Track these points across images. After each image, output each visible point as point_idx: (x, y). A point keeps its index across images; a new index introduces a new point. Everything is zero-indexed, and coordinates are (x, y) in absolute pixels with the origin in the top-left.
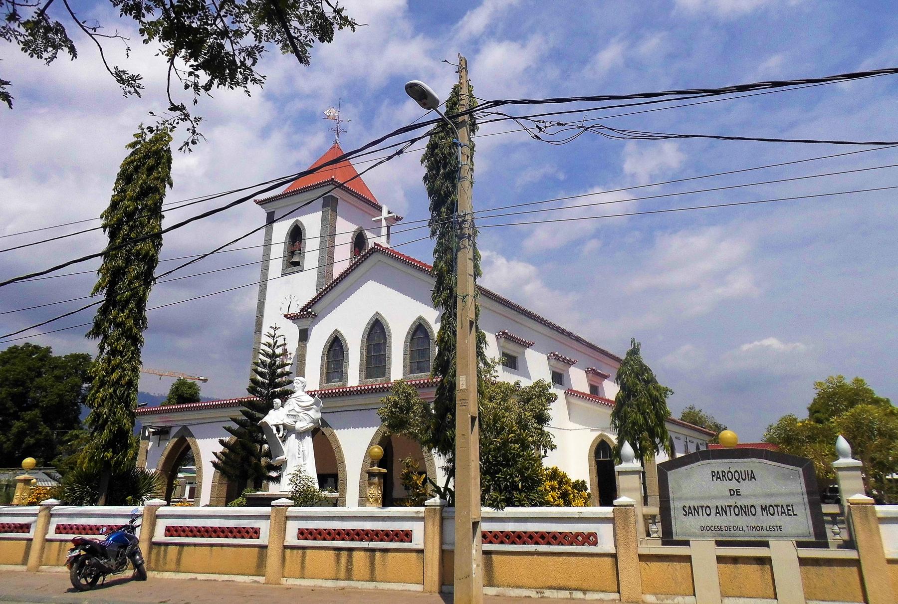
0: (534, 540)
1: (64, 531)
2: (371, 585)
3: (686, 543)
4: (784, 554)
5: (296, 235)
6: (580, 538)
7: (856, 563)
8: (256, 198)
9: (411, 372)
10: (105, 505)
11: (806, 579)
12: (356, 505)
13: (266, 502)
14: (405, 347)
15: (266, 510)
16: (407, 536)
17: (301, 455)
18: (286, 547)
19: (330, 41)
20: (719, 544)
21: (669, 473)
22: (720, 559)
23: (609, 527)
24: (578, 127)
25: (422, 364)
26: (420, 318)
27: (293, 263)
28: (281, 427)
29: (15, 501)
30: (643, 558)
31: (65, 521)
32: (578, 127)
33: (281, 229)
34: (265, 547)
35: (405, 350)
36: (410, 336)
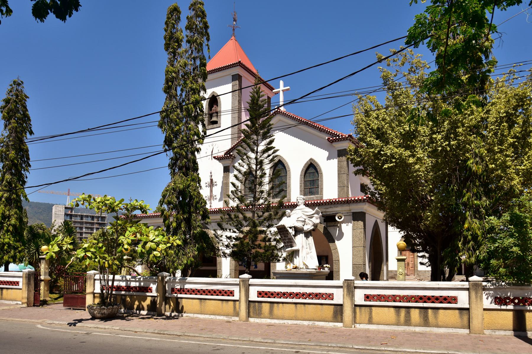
0: (268, 296)
1: (188, 293)
2: (268, 321)
6: (398, 298)
10: (235, 278)
13: (283, 275)
14: (301, 178)
17: (308, 247)
18: (356, 306)
19: (12, 12)
25: (313, 189)
26: (311, 159)
31: (17, 287)
34: (341, 305)
35: (301, 181)
36: (304, 171)
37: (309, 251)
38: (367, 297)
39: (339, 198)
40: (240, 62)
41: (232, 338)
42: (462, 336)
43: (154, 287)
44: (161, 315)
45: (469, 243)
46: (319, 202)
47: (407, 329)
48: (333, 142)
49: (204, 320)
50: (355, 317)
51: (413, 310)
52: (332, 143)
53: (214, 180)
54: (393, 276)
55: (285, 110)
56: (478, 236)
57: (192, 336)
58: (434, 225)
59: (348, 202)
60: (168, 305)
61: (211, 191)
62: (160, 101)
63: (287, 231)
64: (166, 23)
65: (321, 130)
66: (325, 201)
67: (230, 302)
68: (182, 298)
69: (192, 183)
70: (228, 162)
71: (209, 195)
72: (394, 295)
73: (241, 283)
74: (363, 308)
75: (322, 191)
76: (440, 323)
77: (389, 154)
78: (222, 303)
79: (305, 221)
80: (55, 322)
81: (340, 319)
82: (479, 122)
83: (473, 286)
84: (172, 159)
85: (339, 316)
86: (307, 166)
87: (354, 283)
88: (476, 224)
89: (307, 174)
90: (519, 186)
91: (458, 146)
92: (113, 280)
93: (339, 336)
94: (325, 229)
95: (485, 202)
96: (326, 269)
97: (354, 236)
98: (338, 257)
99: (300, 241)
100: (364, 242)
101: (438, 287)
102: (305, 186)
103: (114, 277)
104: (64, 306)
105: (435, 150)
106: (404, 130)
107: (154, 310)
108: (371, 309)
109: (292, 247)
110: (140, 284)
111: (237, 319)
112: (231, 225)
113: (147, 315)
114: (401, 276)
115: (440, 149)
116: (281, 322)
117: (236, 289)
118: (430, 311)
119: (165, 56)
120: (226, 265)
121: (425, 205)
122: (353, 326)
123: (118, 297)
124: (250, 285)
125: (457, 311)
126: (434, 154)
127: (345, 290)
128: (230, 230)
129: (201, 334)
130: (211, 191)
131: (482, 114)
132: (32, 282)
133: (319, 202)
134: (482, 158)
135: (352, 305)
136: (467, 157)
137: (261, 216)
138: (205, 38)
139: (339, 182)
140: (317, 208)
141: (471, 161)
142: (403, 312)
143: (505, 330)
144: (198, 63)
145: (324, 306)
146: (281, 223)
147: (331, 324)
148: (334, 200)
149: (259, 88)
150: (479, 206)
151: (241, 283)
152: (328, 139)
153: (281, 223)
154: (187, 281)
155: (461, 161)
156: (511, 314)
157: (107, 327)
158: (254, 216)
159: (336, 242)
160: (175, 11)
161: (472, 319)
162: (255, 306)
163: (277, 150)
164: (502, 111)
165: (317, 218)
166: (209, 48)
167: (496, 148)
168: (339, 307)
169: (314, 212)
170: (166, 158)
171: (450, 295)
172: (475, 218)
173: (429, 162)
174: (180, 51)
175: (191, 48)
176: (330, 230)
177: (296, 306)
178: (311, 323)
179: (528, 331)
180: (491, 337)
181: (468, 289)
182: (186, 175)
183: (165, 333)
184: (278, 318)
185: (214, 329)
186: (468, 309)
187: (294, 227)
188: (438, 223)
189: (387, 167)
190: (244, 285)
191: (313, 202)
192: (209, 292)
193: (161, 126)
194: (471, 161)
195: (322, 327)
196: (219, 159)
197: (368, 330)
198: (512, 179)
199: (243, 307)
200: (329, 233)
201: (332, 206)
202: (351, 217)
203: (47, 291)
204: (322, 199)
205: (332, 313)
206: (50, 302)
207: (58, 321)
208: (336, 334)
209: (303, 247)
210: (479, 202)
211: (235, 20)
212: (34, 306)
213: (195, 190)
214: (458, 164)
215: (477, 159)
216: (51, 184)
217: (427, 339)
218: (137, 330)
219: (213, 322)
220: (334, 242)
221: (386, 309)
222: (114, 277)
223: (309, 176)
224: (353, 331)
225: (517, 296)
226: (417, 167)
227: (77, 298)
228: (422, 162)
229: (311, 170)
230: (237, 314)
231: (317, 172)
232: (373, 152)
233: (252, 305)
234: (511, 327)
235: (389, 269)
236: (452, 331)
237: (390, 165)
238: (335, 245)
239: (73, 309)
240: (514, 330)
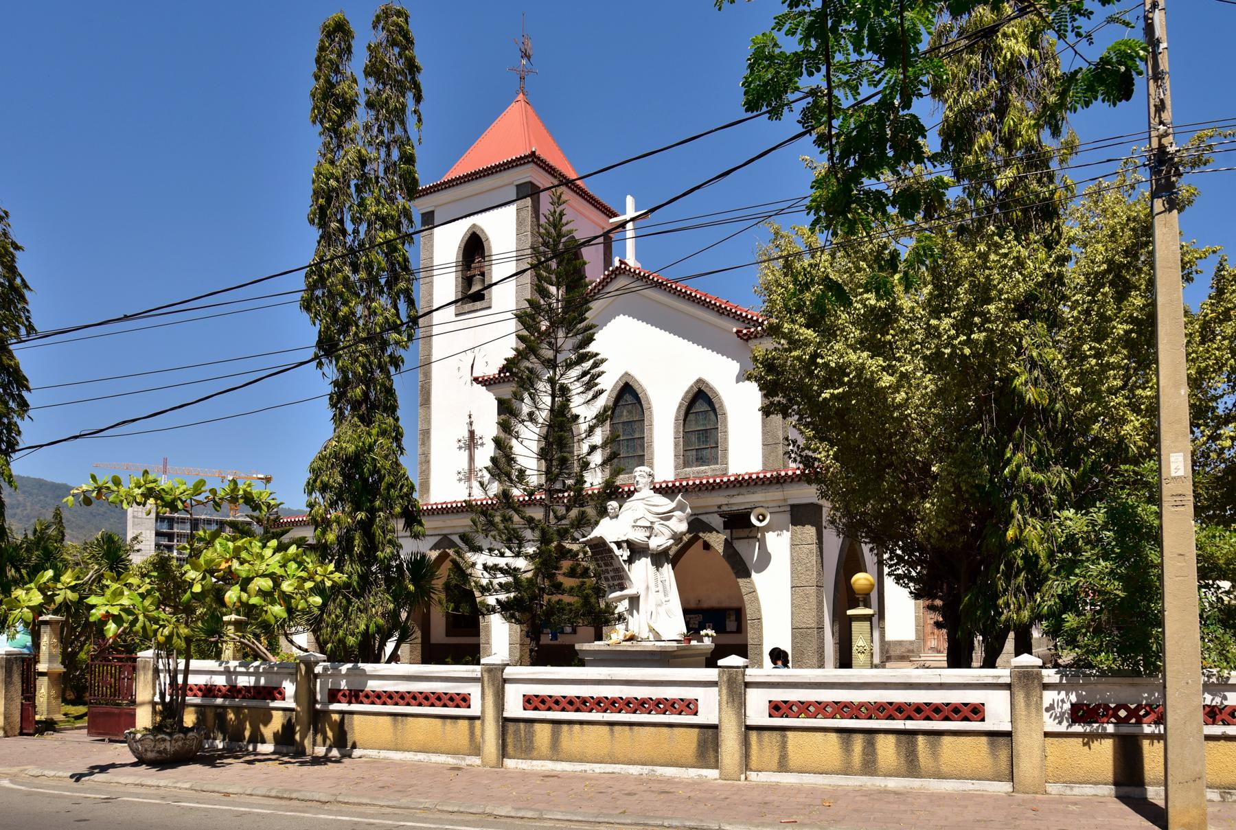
1: (365, 700)
2: (548, 766)
5: (474, 247)
8: (801, 95)
9: (686, 464)
10: (533, 664)
13: (658, 657)
14: (676, 427)
15: (711, 674)
17: (660, 588)
18: (749, 728)
19: (1128, 97)
25: (704, 452)
26: (700, 381)
27: (473, 294)
29: (974, 664)
31: (780, 695)
35: (677, 432)
36: (684, 408)
37: (664, 599)
38: (776, 708)
39: (764, 471)
40: (533, 153)
41: (445, 808)
42: (995, 798)
43: (289, 688)
44: (299, 752)
45: (1017, 575)
46: (711, 481)
47: (869, 784)
48: (749, 338)
49: (400, 765)
50: (747, 755)
51: (881, 738)
52: (747, 340)
53: (478, 434)
54: (890, 654)
55: (639, 265)
56: (1037, 556)
57: (354, 804)
58: (939, 532)
59: (778, 481)
60: (317, 732)
61: (471, 459)
62: (304, 244)
63: (611, 550)
64: (318, 61)
65: (721, 311)
66: (732, 479)
67: (461, 722)
68: (352, 713)
69: (381, 440)
70: (507, 391)
71: (466, 467)
72: (819, 703)
73: (486, 676)
74: (766, 734)
75: (725, 456)
76: (944, 769)
77: (833, 365)
78: (444, 724)
79: (651, 528)
80: (46, 772)
81: (713, 760)
82: (1040, 285)
83: (1019, 678)
84: (336, 383)
85: (712, 754)
86: (690, 395)
87: (744, 675)
88: (1034, 531)
89: (691, 417)
90: (1137, 438)
91: (989, 343)
92: (187, 672)
93: (698, 801)
94: (728, 544)
95: (1059, 475)
96: (707, 641)
97: (795, 562)
98: (759, 610)
99: (641, 573)
100: (819, 574)
101: (938, 681)
102: (686, 443)
103: (187, 665)
104: (89, 733)
105: (938, 354)
106: (865, 306)
107: (288, 744)
108: (785, 736)
109: (622, 588)
110: (257, 681)
111: (476, 761)
112: (494, 537)
113: (273, 753)
114: (861, 657)
115: (948, 351)
116: (579, 767)
117: (474, 691)
118: (920, 739)
119: (313, 138)
120: (500, 635)
121: (920, 481)
122: (743, 777)
123: (208, 711)
124: (505, 681)
125: (984, 739)
126: (935, 363)
127: (724, 691)
128: (491, 550)
129: (375, 798)
130: (471, 459)
131: (1046, 266)
132: (17, 679)
133: (711, 481)
134: (1050, 375)
135: (740, 726)
136: (1012, 371)
137: (564, 517)
138: (410, 95)
139: (764, 433)
140: (679, 497)
141: (1023, 378)
142: (858, 742)
143: (1096, 783)
144: (395, 155)
145: (676, 730)
146: (596, 533)
147: (693, 773)
148: (754, 476)
149: (561, 214)
150: (1042, 484)
151: (486, 679)
152: (738, 332)
153: (596, 533)
155: (1000, 379)
156: (1108, 744)
157: (162, 783)
158: (547, 516)
159: (754, 575)
160: (339, 31)
161: (1018, 757)
162: (517, 732)
163: (603, 361)
164: (1099, 258)
165: (681, 521)
166: (420, 120)
167: (1086, 347)
168: (710, 732)
169: (673, 505)
170: (322, 380)
172: (1033, 515)
173: (929, 382)
174: (349, 126)
175: (377, 119)
176: (740, 546)
177: (612, 731)
178: (645, 770)
179: (1150, 785)
180: (1061, 799)
181: (1008, 686)
182: (367, 420)
183: (294, 795)
184: (570, 760)
185: (411, 786)
186: (1008, 734)
187: (627, 541)
188: (950, 530)
189: (828, 395)
190: (493, 679)
191: (697, 482)
192: (439, 698)
193: (307, 306)
194: (1023, 378)
195: (670, 781)
196: (487, 383)
197: (774, 787)
198: (1123, 421)
199: (490, 734)
200: (736, 553)
201: (743, 490)
202: (787, 517)
203: (56, 698)
204: (725, 475)
205: (694, 745)
206: (62, 725)
207: (54, 769)
208: (698, 795)
209: (648, 588)
210: (1041, 477)
211: (526, 55)
212: (21, 734)
213: (386, 457)
214: (992, 387)
215: (1036, 373)
216: (41, 446)
217: (903, 808)
218: (230, 791)
219: (417, 768)
220: (749, 575)
221: (819, 735)
222: (187, 665)
223: (697, 421)
224: (739, 789)
225: (1123, 702)
226: (900, 397)
227: (119, 715)
228: (910, 385)
229: (701, 405)
230: (476, 750)
231: (714, 410)
232: (799, 358)
233: (511, 727)
234: (1110, 776)
235: (887, 638)
236: (971, 787)
237: (836, 392)
238: (752, 583)
239: (111, 741)
240: (1116, 784)
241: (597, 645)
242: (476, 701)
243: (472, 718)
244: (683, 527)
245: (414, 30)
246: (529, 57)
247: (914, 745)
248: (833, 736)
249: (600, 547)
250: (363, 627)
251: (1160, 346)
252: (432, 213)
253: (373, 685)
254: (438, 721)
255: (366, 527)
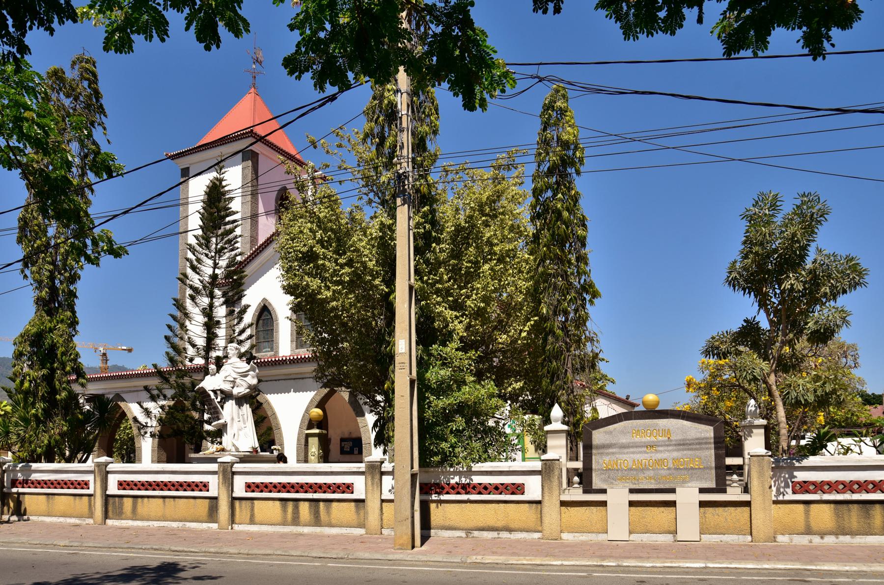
3: (604, 491)
4: (688, 496)
5: (216, 196)
7: (748, 504)
11: (703, 517)
12: (298, 463)
15: (214, 467)
16: (348, 488)
17: (241, 419)
20: (632, 491)
21: (594, 432)
22: (632, 504)
23: (538, 478)
24: (532, 77)
28: (219, 392)
30: (563, 504)
32: (532, 77)
33: (198, 187)
34: (216, 498)
37: (243, 426)
38: (249, 487)
63: (209, 396)
68: (24, 494)
74: (244, 502)
76: (333, 521)
79: (234, 382)
99: (229, 410)
101: (329, 470)
111: (91, 521)
114: (313, 458)
118: (321, 504)
124: (108, 472)
125: (353, 504)
145: (198, 500)
147: (205, 526)
154: (33, 468)
162: (114, 503)
165: (253, 377)
171: (491, 482)
177: (837, 515)
178: (180, 524)
179: (434, 529)
184: (142, 520)
190: (100, 471)
205: (207, 509)
208: (212, 538)
209: (233, 419)
211: (257, 61)
220: (363, 415)
221: (271, 502)
230: (91, 515)
233: (111, 500)
238: (365, 420)
241: (197, 455)
242: (92, 485)
243: (90, 495)
244: (254, 381)
245: (99, 71)
246: (260, 63)
247: (318, 507)
248: (278, 503)
249: (203, 392)
250: (46, 442)
251: (397, 285)
252: (188, 168)
253: (35, 477)
254: (72, 498)
255: (49, 379)
